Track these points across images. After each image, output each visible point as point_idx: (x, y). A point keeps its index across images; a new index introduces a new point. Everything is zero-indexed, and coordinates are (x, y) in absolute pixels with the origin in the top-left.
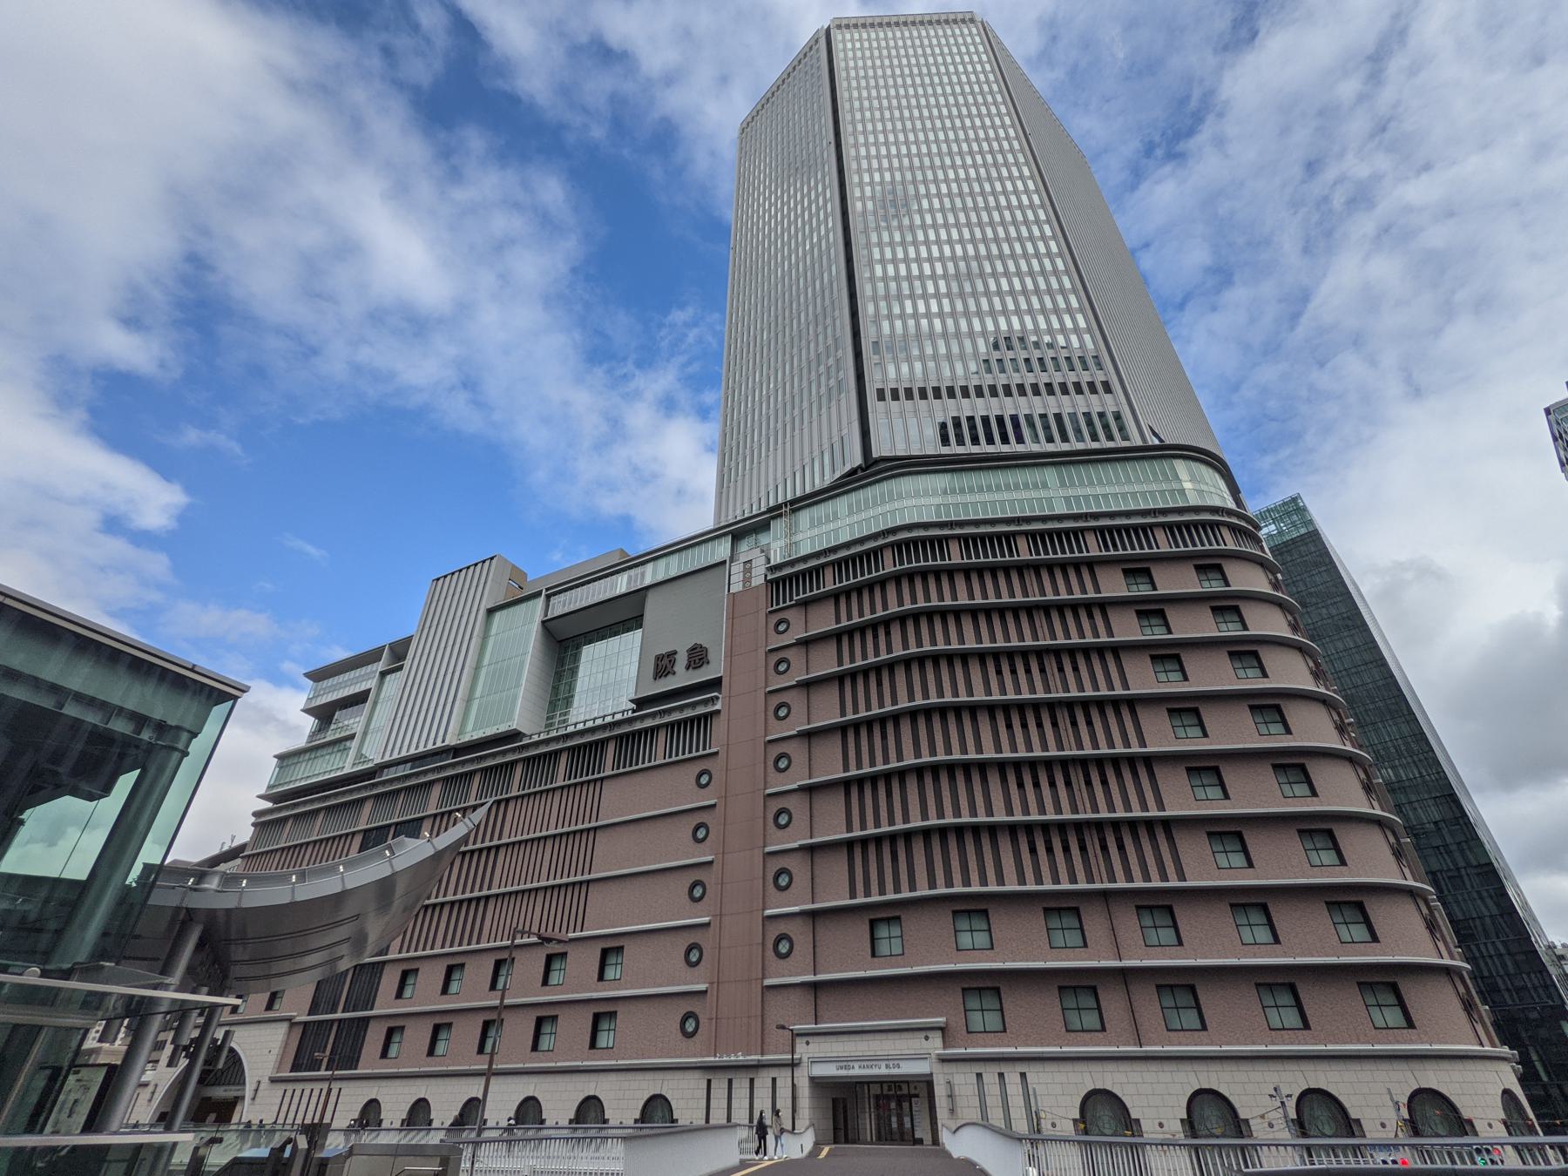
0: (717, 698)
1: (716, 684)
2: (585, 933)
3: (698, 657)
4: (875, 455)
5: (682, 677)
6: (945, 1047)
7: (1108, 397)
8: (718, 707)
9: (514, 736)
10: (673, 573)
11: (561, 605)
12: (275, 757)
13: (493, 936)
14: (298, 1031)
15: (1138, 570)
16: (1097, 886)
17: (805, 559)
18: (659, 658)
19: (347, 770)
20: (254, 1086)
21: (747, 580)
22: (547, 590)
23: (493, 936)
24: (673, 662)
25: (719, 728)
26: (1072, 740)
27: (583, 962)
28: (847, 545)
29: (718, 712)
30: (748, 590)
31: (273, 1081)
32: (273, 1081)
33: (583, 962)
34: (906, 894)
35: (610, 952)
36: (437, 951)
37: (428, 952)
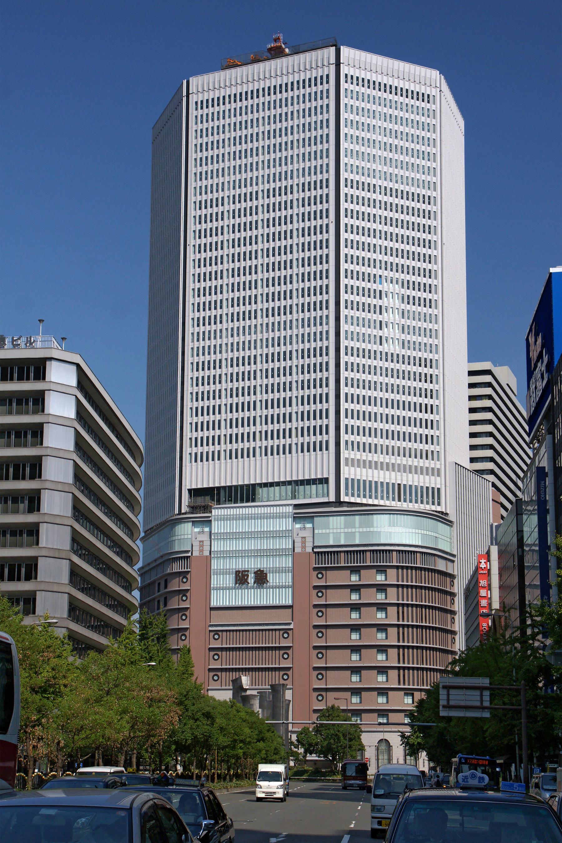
18: (237, 572)
21: (304, 547)
24: (248, 576)
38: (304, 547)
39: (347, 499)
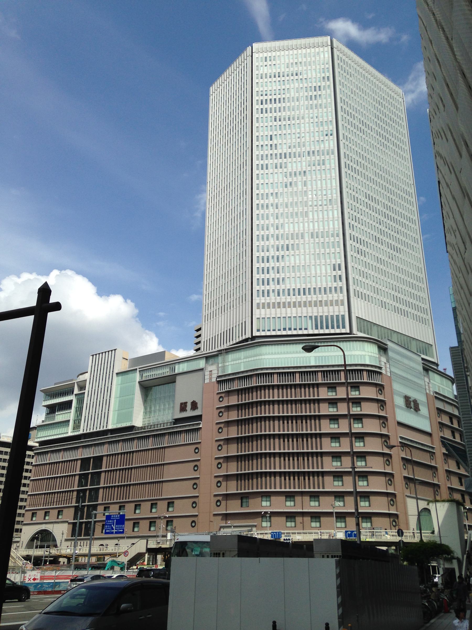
1: (199, 417)
2: (162, 497)
3: (194, 406)
4: (254, 335)
5: (189, 413)
8: (201, 426)
10: (185, 370)
11: (148, 375)
12: (339, 628)
13: (104, 499)
14: (71, 526)
16: (300, 490)
17: (229, 375)
19: (70, 434)
20: (60, 541)
21: (211, 379)
22: (139, 368)
23: (104, 499)
24: (186, 406)
25: (202, 432)
26: (301, 446)
27: (162, 505)
28: (243, 372)
29: (201, 428)
30: (211, 382)
31: (66, 540)
32: (66, 540)
33: (162, 505)
34: (273, 490)
35: (170, 503)
36: (55, 506)
37: (52, 507)
38: (211, 379)
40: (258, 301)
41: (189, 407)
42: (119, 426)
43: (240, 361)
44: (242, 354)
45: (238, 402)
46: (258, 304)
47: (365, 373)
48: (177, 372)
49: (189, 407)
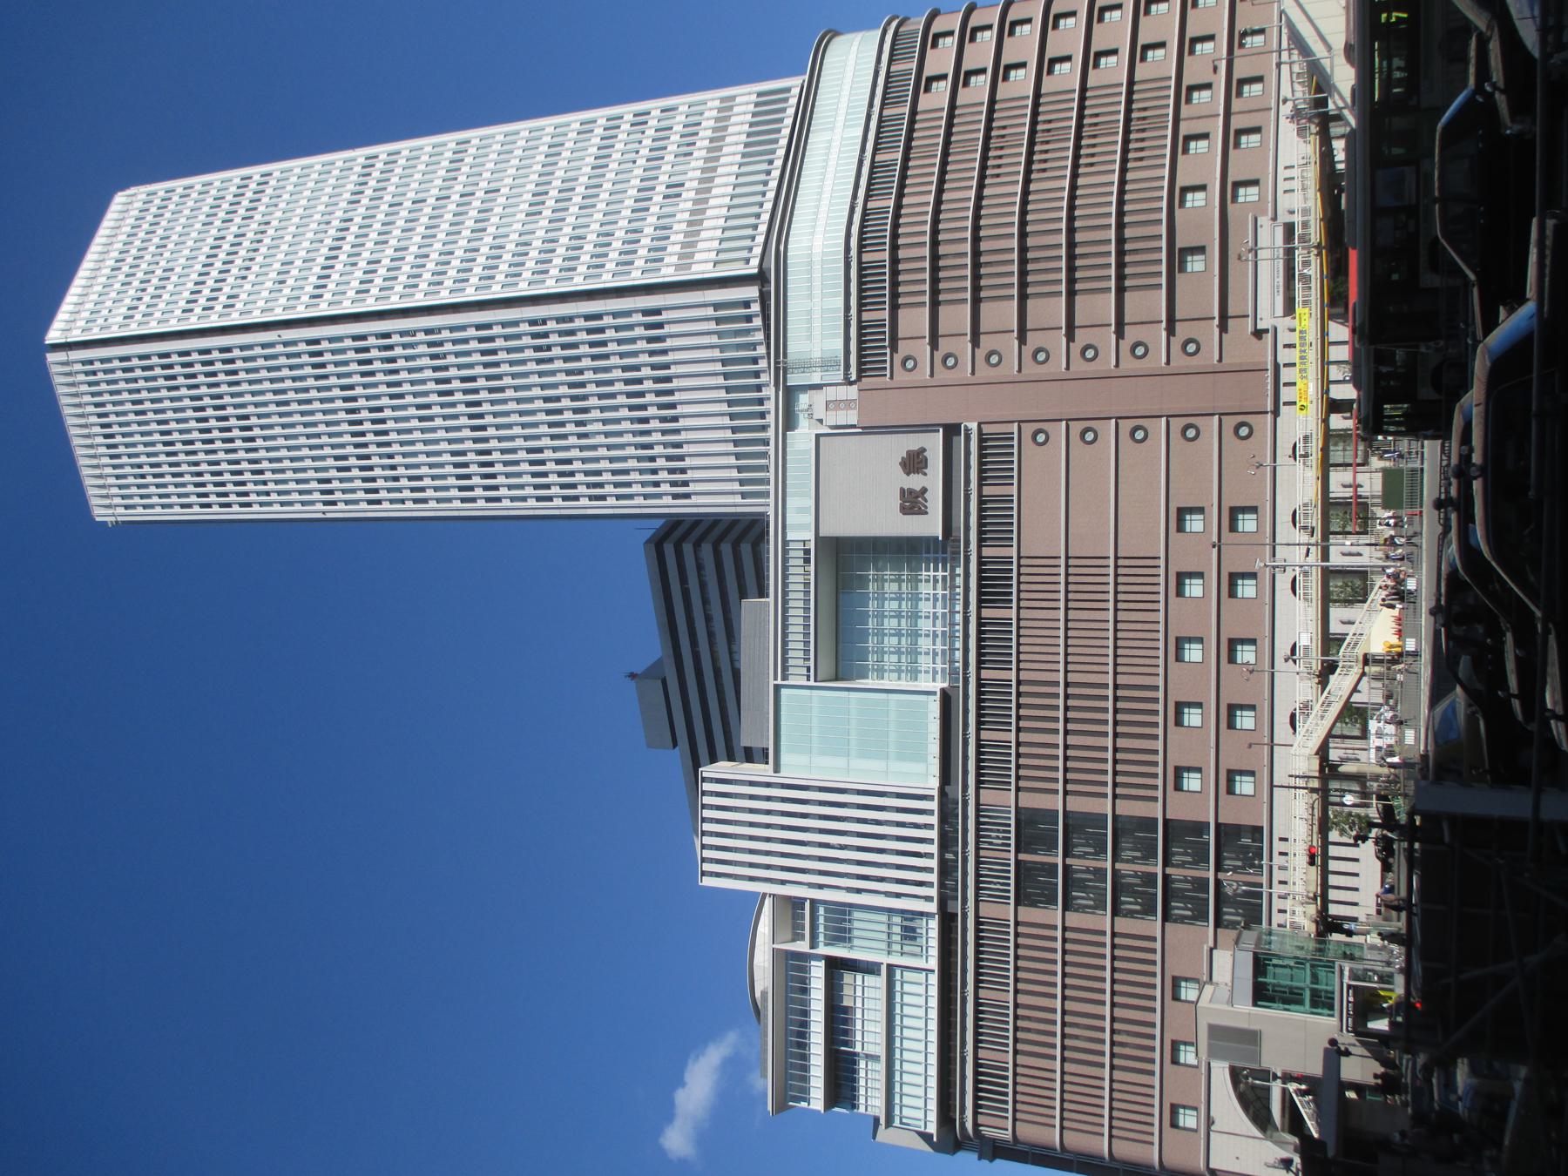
0: (965, 426)
3: (914, 462)
6: (1267, 214)
7: (738, 100)
8: (974, 426)
9: (946, 699)
15: (925, 83)
21: (847, 404)
24: (911, 491)
38: (847, 404)
39: (755, 262)
40: (671, 270)
41: (915, 482)
42: (934, 748)
43: (817, 316)
44: (796, 305)
45: (1056, 792)
46: (678, 267)
47: (866, 257)
48: (810, 536)
49: (915, 482)
